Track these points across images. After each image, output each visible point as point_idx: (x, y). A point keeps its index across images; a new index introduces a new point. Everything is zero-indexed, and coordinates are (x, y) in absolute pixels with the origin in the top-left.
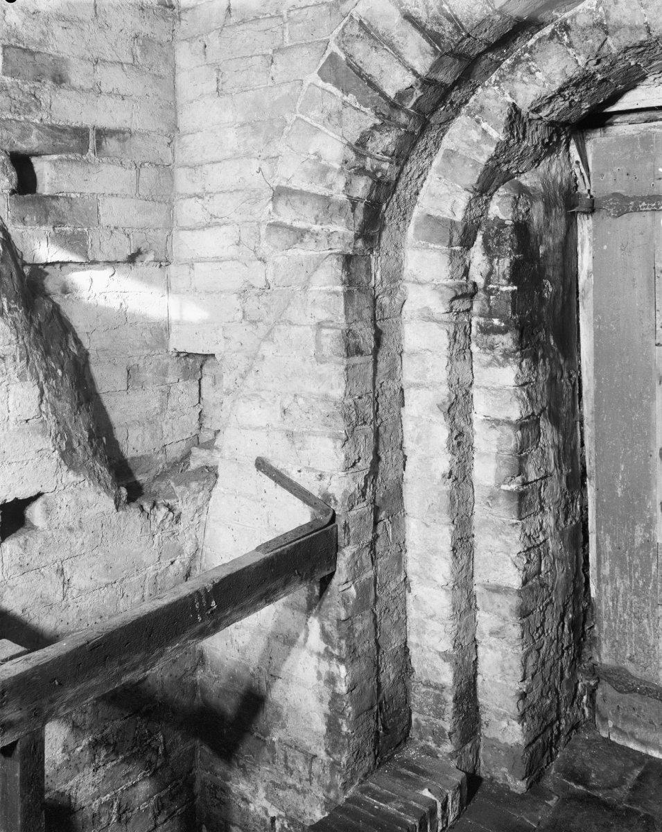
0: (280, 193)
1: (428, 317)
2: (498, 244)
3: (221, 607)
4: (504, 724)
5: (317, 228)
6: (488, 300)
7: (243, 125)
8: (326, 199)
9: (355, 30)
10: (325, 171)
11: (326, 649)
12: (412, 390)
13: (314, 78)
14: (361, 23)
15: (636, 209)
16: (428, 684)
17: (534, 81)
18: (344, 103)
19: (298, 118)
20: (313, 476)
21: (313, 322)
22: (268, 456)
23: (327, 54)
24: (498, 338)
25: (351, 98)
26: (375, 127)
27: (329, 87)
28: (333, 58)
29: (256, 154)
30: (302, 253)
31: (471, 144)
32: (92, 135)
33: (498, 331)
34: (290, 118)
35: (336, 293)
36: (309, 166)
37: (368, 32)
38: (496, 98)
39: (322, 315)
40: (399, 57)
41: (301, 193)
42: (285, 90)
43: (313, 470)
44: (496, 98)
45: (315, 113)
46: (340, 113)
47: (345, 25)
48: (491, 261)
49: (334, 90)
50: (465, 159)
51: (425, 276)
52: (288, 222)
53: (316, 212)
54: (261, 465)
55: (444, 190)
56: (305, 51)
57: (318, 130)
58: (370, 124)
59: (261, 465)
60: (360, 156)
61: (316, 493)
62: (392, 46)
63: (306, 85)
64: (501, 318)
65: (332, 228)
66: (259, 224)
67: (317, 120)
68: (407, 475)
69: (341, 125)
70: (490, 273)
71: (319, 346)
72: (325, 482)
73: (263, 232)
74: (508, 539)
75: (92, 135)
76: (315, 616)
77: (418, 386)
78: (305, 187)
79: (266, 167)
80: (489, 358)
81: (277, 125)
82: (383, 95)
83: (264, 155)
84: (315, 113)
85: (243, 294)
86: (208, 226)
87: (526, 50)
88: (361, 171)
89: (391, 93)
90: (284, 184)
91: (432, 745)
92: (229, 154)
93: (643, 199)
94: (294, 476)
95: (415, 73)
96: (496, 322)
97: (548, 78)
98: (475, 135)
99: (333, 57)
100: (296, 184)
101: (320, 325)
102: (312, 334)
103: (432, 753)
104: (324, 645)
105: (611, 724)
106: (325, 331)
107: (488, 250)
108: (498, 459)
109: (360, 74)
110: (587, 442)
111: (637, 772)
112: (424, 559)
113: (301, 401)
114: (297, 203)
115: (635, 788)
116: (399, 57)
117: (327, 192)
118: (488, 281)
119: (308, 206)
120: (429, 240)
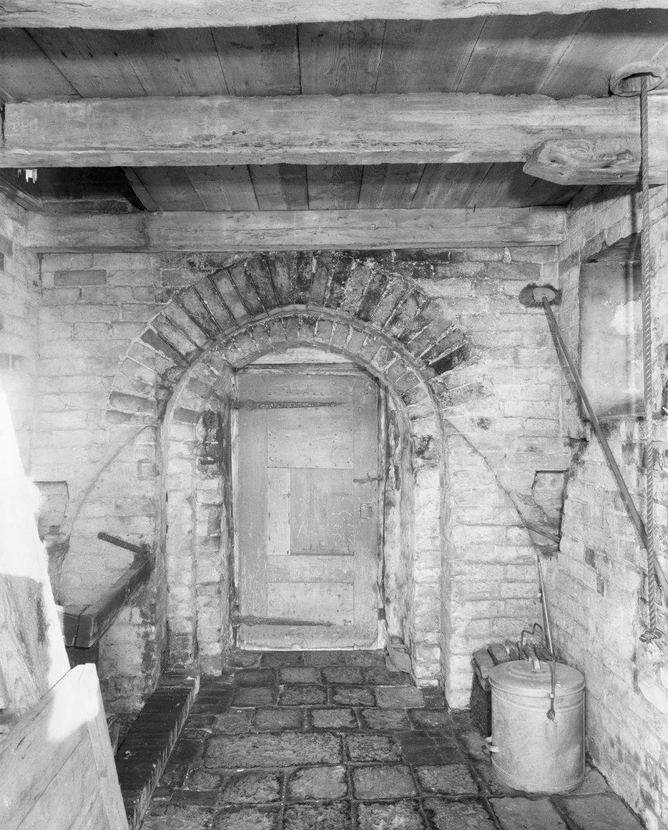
0: (115, 395)
1: (180, 457)
2: (211, 422)
3: (131, 591)
4: (211, 646)
5: (138, 413)
6: (205, 449)
7: (89, 358)
8: (145, 400)
9: (164, 321)
10: (144, 386)
11: (143, 621)
12: (172, 493)
13: (138, 339)
14: (166, 318)
15: (259, 407)
16: (179, 635)
17: (237, 352)
18: (156, 354)
19: (127, 359)
20: (136, 537)
21: (137, 460)
22: (106, 531)
23: (146, 329)
24: (210, 466)
25: (160, 352)
26: (173, 367)
27: (147, 345)
28: (150, 331)
29: (99, 373)
30: (128, 426)
31: (205, 376)
32: (10, 357)
33: (210, 463)
34: (122, 358)
35: (151, 446)
36: (135, 383)
37: (170, 322)
38: (218, 357)
39: (142, 457)
40: (188, 337)
41: (129, 396)
42: (120, 343)
43: (136, 534)
44: (218, 357)
45: (139, 357)
46: (154, 359)
47: (157, 317)
48: (207, 431)
49: (150, 347)
50: (201, 383)
51: (180, 437)
52: (120, 410)
53: (138, 406)
54: (102, 536)
55: (190, 397)
56: (133, 326)
57: (140, 366)
58: (171, 366)
59: (102, 536)
60: (163, 380)
61: (138, 545)
62: (184, 331)
63: (132, 343)
64: (211, 456)
65: (146, 414)
66: (101, 411)
67: (139, 360)
68: (168, 535)
69: (154, 364)
70: (207, 436)
71: (140, 472)
72: (143, 539)
73: (104, 414)
74: (214, 559)
75: (10, 357)
76: (136, 606)
77: (176, 491)
78: (132, 393)
79: (105, 380)
80: (205, 476)
81: (114, 360)
82: (179, 353)
83: (104, 375)
84: (139, 357)
85: (88, 447)
86: (62, 411)
87: (233, 337)
88: (162, 387)
89: (184, 353)
90: (117, 390)
91: (181, 663)
92: (79, 372)
93: (263, 403)
94: (124, 538)
95: (196, 345)
96: (209, 459)
97: (243, 351)
98: (207, 372)
99: (150, 331)
100: (125, 391)
101: (140, 462)
102: (136, 466)
103: (182, 667)
104: (142, 619)
105: (245, 642)
106: (143, 465)
107: (205, 425)
108: (209, 522)
109: (165, 341)
110: (234, 515)
111: (260, 657)
112: (177, 575)
113: (129, 500)
114: (127, 401)
115: (261, 662)
116: (188, 337)
117: (145, 396)
118: (205, 440)
119: (134, 403)
120: (182, 420)
